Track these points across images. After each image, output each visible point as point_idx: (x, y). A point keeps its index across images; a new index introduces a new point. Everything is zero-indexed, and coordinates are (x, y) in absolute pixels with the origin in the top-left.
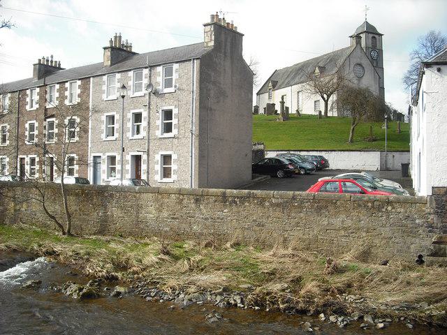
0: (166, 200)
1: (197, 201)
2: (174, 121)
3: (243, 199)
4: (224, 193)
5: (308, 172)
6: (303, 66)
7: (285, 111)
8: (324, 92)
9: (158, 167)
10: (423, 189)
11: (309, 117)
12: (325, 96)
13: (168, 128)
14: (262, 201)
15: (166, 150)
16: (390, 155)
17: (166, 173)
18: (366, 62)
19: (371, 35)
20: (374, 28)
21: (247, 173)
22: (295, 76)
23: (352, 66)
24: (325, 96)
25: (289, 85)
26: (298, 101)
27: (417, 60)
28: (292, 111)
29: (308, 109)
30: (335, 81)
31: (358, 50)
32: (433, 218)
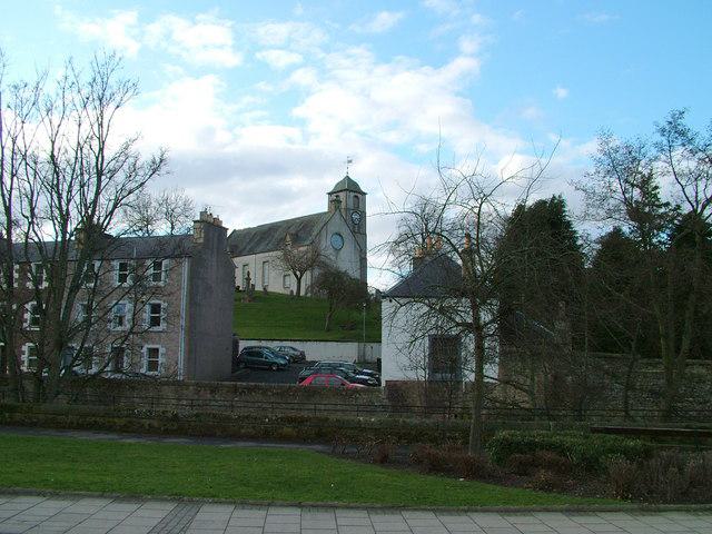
0: (185, 391)
1: (212, 392)
2: (163, 315)
3: (250, 390)
4: (236, 386)
5: (280, 368)
6: (270, 229)
7: (250, 289)
8: (298, 268)
9: (145, 362)
10: (385, 378)
11: (278, 297)
12: (298, 273)
13: (155, 322)
14: (265, 391)
15: (153, 343)
16: (369, 346)
17: (153, 365)
18: (346, 232)
19: (352, 194)
20: (355, 184)
21: (228, 366)
22: (258, 243)
23: (329, 237)
24: (298, 273)
25: (251, 252)
26: (263, 276)
27: (405, 228)
28: (259, 288)
29: (276, 287)
30: (309, 255)
31: (337, 216)
32: (386, 402)
